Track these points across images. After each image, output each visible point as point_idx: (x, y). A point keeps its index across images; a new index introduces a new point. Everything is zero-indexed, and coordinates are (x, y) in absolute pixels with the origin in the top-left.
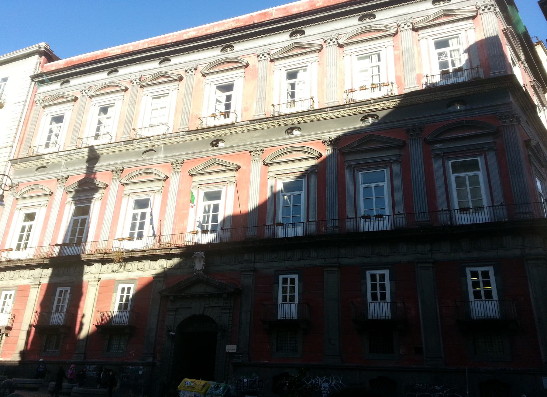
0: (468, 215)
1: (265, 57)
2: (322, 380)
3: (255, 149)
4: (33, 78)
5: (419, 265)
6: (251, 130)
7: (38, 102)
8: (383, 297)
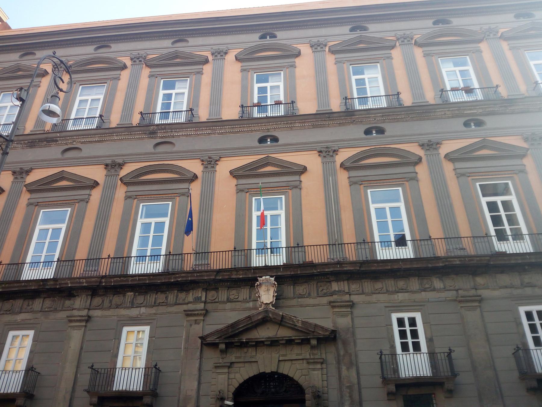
0: (391, 250)
1: (140, 61)
8: (417, 347)
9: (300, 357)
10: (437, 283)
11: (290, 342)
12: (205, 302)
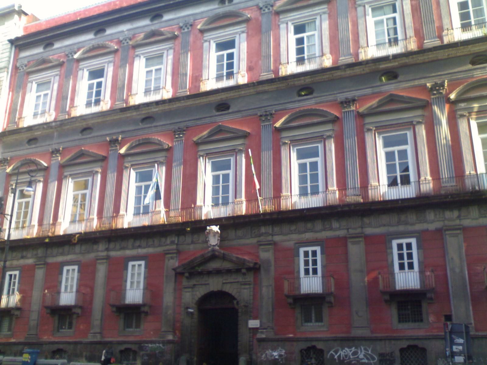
2: (351, 351)
3: (264, 114)
4: (11, 42)
5: (447, 232)
6: (258, 93)
7: (20, 68)
9: (237, 281)
10: (335, 225)
11: (229, 272)
12: (177, 244)
